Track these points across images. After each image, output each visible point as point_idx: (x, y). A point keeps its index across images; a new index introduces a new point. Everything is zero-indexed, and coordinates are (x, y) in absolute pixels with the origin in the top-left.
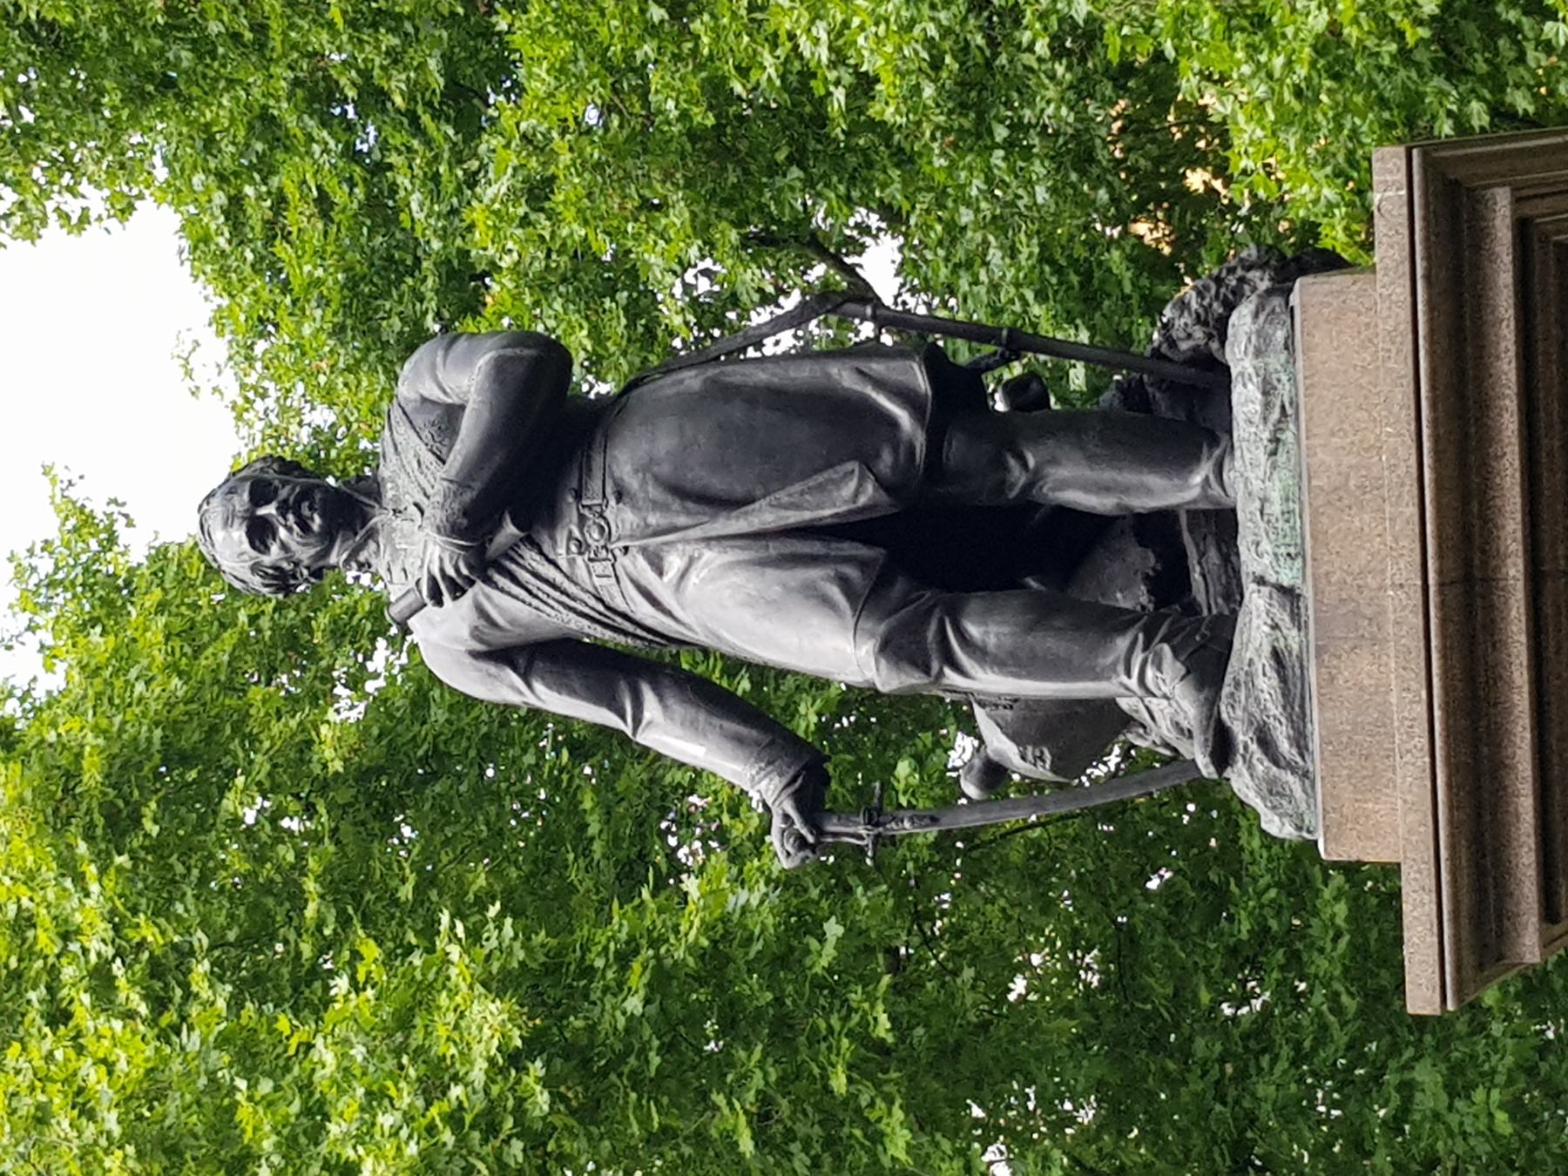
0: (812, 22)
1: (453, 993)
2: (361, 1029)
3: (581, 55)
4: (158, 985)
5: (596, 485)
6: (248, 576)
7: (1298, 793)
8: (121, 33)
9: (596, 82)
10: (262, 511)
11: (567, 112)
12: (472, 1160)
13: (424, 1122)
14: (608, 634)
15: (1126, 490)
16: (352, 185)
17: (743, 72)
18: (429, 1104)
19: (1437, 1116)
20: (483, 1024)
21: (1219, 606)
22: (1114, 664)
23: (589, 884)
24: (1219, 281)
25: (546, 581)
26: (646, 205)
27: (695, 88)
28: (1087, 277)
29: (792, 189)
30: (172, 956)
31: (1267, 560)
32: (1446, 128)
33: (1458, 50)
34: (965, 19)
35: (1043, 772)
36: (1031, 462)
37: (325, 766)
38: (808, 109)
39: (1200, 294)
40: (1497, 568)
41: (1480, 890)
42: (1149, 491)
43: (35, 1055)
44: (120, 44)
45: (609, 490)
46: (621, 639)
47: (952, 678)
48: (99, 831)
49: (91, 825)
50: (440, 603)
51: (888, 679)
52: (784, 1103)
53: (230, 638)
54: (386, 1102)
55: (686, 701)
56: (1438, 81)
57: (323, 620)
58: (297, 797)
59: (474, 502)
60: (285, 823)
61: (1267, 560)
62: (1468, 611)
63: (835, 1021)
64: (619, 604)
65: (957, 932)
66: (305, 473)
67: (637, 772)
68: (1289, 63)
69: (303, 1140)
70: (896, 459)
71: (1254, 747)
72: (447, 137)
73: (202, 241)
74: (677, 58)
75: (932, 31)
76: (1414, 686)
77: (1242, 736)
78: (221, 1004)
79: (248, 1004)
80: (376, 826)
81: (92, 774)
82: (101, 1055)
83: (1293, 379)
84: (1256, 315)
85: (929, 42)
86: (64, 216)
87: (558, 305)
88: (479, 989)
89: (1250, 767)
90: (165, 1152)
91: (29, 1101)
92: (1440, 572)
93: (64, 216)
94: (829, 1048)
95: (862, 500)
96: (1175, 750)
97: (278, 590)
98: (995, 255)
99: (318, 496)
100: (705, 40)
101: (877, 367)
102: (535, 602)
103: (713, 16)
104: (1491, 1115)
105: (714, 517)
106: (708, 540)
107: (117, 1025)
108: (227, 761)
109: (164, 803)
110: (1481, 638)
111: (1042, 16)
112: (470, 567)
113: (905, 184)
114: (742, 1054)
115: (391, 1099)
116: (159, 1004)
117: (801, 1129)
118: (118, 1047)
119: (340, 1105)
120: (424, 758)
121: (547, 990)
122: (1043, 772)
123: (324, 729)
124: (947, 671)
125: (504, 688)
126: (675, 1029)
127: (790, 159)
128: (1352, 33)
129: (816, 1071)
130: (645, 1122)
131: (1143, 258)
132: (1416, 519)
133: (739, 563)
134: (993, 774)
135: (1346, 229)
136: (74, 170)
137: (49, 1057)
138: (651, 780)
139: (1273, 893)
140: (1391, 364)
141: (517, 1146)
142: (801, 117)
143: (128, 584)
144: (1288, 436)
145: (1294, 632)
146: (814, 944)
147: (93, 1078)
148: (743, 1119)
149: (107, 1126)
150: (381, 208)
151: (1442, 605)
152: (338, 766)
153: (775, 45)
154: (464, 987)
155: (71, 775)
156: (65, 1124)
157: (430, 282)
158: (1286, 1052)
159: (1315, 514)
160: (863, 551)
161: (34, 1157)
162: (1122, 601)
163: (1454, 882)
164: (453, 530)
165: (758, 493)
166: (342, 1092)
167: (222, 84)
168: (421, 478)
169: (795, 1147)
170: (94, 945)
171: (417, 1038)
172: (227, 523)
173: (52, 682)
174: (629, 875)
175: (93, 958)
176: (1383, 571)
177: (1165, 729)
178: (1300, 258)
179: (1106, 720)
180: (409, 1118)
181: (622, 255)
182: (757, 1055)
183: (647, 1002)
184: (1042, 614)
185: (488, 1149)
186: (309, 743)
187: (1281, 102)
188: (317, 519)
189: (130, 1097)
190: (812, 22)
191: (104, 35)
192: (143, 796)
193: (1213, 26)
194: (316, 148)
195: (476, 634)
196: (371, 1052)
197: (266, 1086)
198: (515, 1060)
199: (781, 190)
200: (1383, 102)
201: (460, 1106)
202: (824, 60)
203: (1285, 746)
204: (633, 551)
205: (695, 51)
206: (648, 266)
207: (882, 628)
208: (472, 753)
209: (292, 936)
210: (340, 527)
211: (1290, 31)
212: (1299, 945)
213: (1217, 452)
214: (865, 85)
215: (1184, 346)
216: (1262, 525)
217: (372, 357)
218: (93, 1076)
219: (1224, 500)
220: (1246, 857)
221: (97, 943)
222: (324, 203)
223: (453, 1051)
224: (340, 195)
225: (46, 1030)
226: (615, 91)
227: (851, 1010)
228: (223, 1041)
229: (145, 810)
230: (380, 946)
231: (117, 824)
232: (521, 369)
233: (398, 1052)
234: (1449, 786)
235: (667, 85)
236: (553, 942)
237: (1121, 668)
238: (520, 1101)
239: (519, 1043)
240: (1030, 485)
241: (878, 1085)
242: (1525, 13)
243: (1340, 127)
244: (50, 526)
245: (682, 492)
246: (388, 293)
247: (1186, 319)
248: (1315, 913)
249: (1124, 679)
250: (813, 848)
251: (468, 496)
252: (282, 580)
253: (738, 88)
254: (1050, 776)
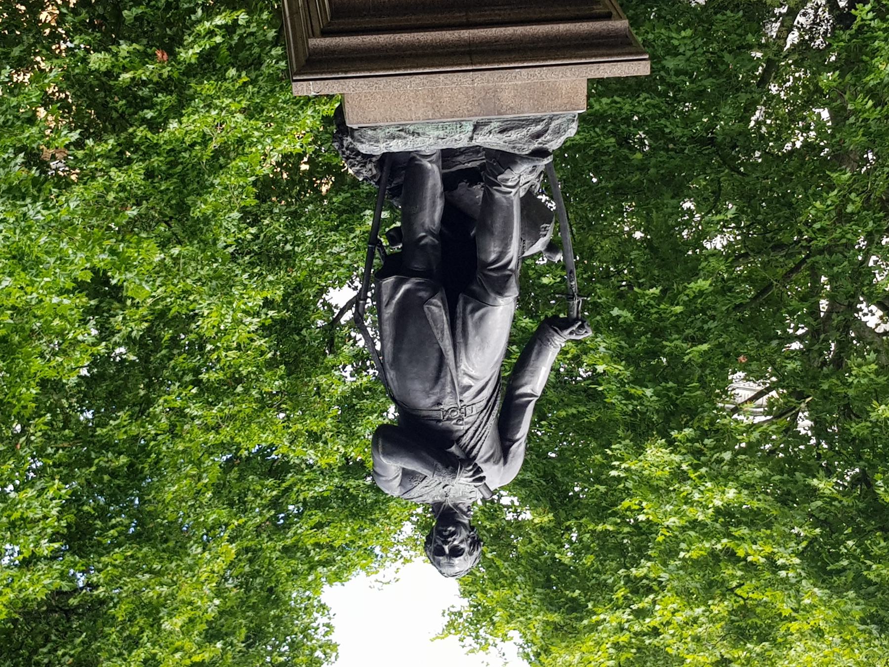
0: (244, 324)
1: (644, 469)
2: (659, 507)
3: (257, 420)
4: (641, 590)
5: (434, 414)
6: (474, 557)
7: (559, 121)
8: (248, 607)
9: (268, 414)
10: (447, 551)
11: (280, 426)
12: (713, 460)
13: (697, 480)
14: (496, 408)
15: (434, 196)
16: (312, 514)
17: (263, 353)
18: (689, 478)
19: (688, 60)
20: (656, 456)
21: (482, 156)
22: (506, 198)
23: (597, 413)
24: (347, 158)
25: (474, 434)
26: (318, 393)
27: (270, 373)
28: (345, 211)
29: (311, 333)
30: (629, 584)
31: (462, 136)
32: (283, 64)
33: (250, 61)
34: (239, 264)
35: (551, 227)
36: (423, 234)
37: (550, 521)
38: (278, 327)
39: (353, 166)
40: (465, 41)
41: (598, 46)
42: (435, 185)
43: (671, 642)
44: (253, 607)
45: (437, 408)
46: (498, 402)
47: (512, 266)
48: (579, 615)
49: (576, 618)
50: (484, 478)
51: (513, 292)
52: (687, 331)
53: (499, 562)
54: (689, 496)
55: (523, 376)
56: (263, 68)
57: (487, 524)
58: (563, 534)
59: (443, 464)
60: (574, 539)
61: (462, 136)
62: (482, 53)
63: (653, 311)
64: (484, 403)
65: (616, 262)
66: (431, 534)
67: (551, 394)
68: (257, 129)
69: (705, 530)
70: (424, 290)
71: (540, 140)
72: (292, 477)
73: (338, 577)
74: (257, 380)
75: (246, 276)
76: (514, 74)
78: (649, 564)
79: (649, 553)
80: (575, 501)
81: (556, 617)
82: (670, 615)
83: (388, 127)
84: (362, 143)
85: (251, 277)
86: (326, 634)
87: (360, 429)
88: (641, 457)
89: (548, 141)
90: (710, 588)
91: (690, 645)
92: (467, 64)
93: (326, 634)
94: (664, 313)
95: (440, 304)
96: (541, 173)
97: (479, 544)
98: (335, 250)
99: (440, 528)
100: (250, 369)
101: (385, 298)
102: (483, 438)
103: (240, 366)
104: (684, 38)
105: (447, 365)
106: (457, 367)
107: (657, 607)
108: (549, 562)
109: (567, 588)
110: (493, 47)
111: (240, 231)
112: (469, 465)
113: (308, 287)
114: (667, 349)
115: (688, 494)
116: (649, 590)
117: (698, 324)
118: (666, 607)
119: (691, 515)
120: (545, 483)
121: (641, 430)
122: (551, 227)
123: (536, 521)
124: (510, 267)
125: (519, 450)
126: (656, 377)
127: (299, 334)
128: (244, 104)
129: (673, 318)
130: (696, 389)
131: (336, 189)
132: (445, 75)
133: (467, 357)
134: (552, 247)
135: (324, 105)
136: (307, 628)
137: (673, 635)
138: (554, 387)
139: (597, 130)
140: (381, 86)
141: (707, 441)
142: (281, 330)
143: (475, 607)
144: (412, 128)
145: (492, 124)
146: (621, 320)
147: (681, 618)
148: (694, 348)
149: (701, 612)
150: (320, 503)
151: (481, 63)
152: (551, 515)
153: (252, 340)
154: (640, 464)
155: (557, 627)
156: (700, 630)
157: (351, 483)
158: (663, 121)
159: (442, 117)
160: (461, 302)
161: (714, 642)
162: (480, 195)
163: (596, 56)
164: (454, 472)
165: (436, 346)
166: (685, 515)
167: (270, 567)
168: (433, 486)
169: (706, 327)
170: (625, 617)
171: (662, 484)
172: (452, 566)
173: (516, 635)
174: (593, 396)
175: (631, 617)
176: (467, 88)
177: (532, 177)
178: (338, 125)
179: (529, 200)
180: (696, 487)
181: (338, 402)
182: (668, 344)
183: (647, 387)
184: (486, 229)
185: (708, 453)
186: (541, 528)
187: (273, 132)
188: (450, 528)
189: (688, 602)
190: (244, 324)
191: (250, 613)
192: (561, 595)
193: (242, 161)
194: (299, 531)
195: (496, 462)
196: (668, 503)
197: (683, 546)
198: (671, 443)
199: (311, 338)
200: (272, 91)
201: (690, 465)
202: (258, 320)
203: (539, 127)
204: (461, 398)
205: (254, 373)
206: (343, 391)
207: (493, 295)
208: (544, 461)
209: (621, 536)
210: (454, 519)
211: (244, 129)
212: (619, 119)
213: (418, 157)
214: (268, 304)
215: (374, 172)
216: (448, 138)
217: (383, 507)
218: (680, 618)
219: (437, 154)
220: (582, 142)
221: (625, 616)
222: (319, 526)
223: (667, 468)
224: (316, 519)
225: (661, 637)
226: (271, 407)
227: (648, 304)
228: (665, 564)
229: (570, 596)
230: (624, 500)
231: (576, 608)
232: (387, 445)
233: (668, 492)
234: (555, 59)
235: (269, 385)
236: (622, 428)
237: (508, 196)
238: (688, 440)
239: (663, 440)
240: (433, 234)
241: (680, 293)
242: (235, 32)
243: (283, 108)
244: (453, 639)
245: (437, 378)
246: (358, 504)
247: (363, 171)
248: (605, 111)
249: (512, 194)
250: (583, 322)
251: (440, 466)
252: (475, 543)
253: (270, 355)
254: (553, 224)
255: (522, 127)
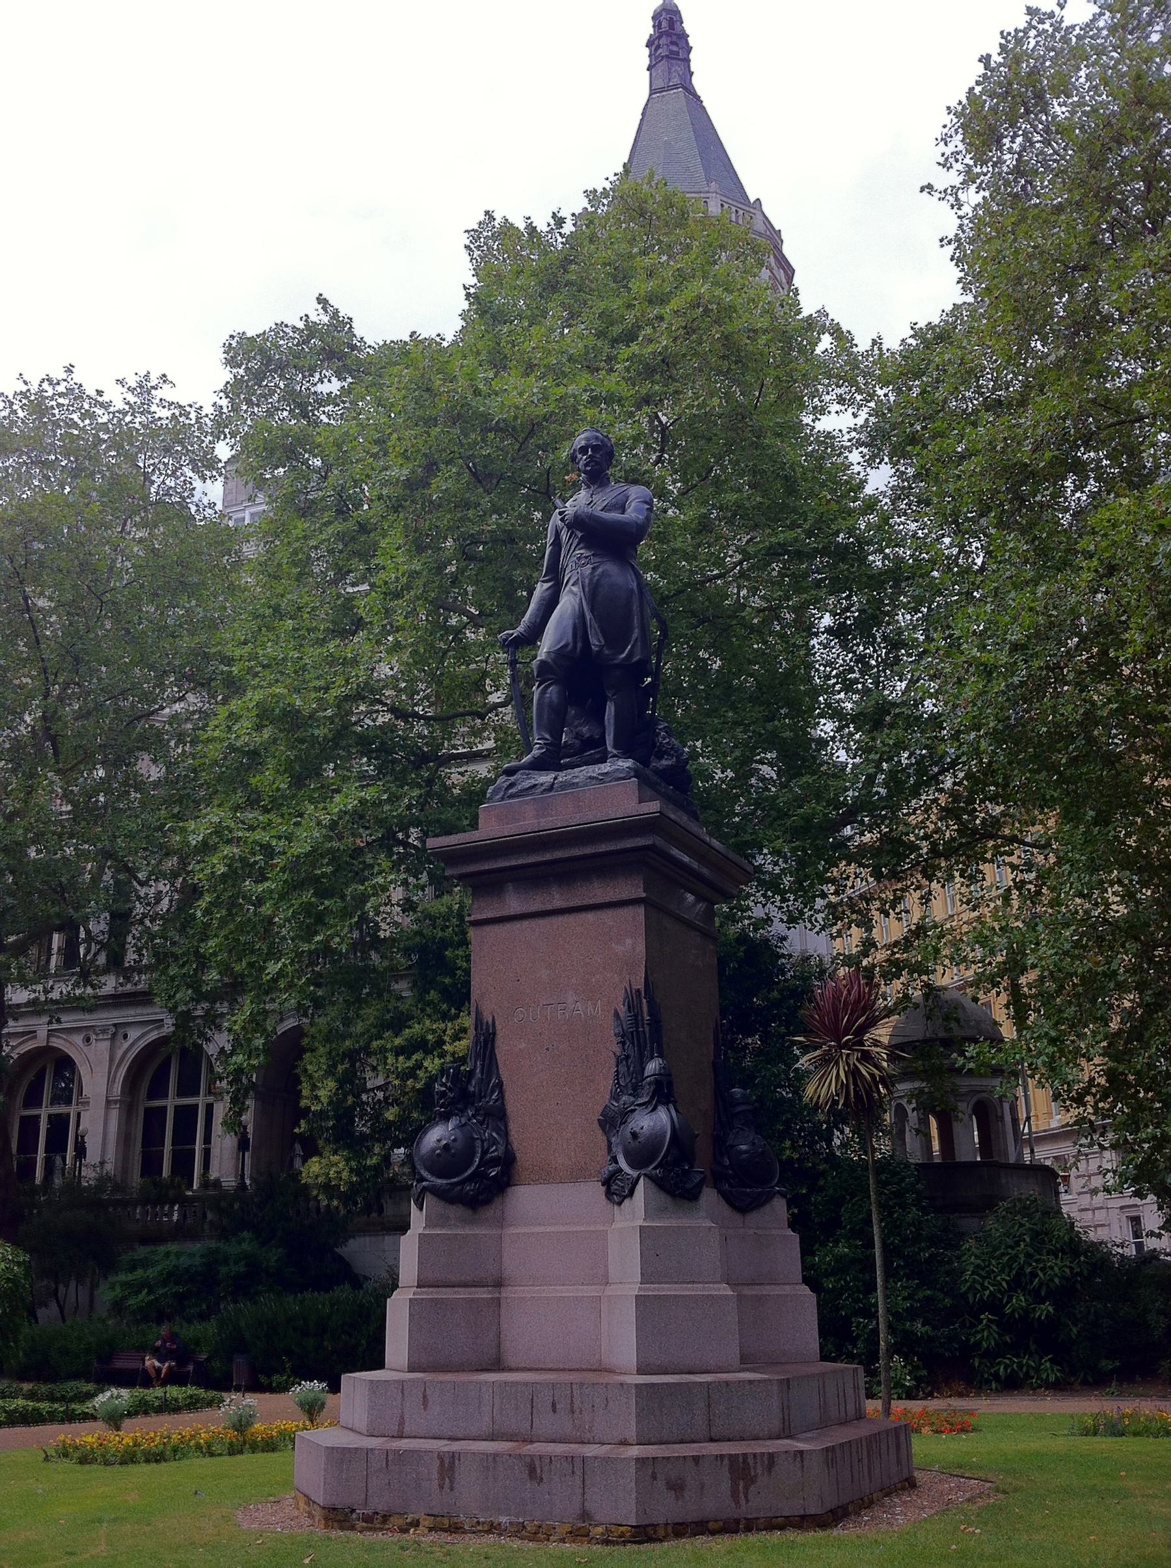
77: (512, 779)
255: (521, 791)
